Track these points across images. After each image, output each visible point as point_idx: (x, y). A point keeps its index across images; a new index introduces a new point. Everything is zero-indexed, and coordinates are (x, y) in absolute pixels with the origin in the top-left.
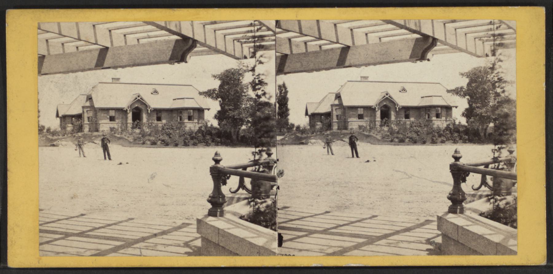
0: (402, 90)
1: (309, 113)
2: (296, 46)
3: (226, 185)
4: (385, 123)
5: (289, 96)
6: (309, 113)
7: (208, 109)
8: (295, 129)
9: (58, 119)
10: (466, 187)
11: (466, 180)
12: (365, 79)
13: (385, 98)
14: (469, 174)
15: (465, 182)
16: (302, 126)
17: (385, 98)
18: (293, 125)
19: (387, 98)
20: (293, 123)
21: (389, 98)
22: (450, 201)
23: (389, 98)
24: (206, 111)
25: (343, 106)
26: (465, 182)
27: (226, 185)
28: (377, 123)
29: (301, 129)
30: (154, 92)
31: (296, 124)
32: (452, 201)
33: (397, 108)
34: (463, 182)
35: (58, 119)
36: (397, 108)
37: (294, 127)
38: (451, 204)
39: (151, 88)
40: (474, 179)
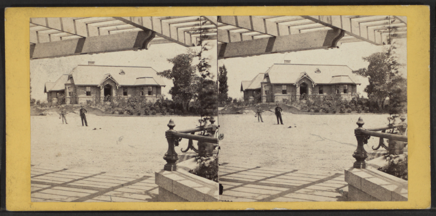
0: (317, 71)
1: (244, 89)
2: (233, 36)
3: (178, 146)
4: (108, 99)
5: (228, 75)
6: (244, 89)
7: (164, 86)
8: (232, 102)
9: (46, 94)
10: (367, 148)
11: (367, 142)
12: (287, 62)
13: (303, 77)
14: (370, 137)
15: (367, 144)
16: (238, 99)
17: (303, 77)
18: (231, 99)
19: (305, 77)
20: (231, 97)
21: (307, 77)
22: (355, 159)
23: (307, 77)
24: (162, 88)
25: (271, 83)
26: (367, 144)
27: (178, 146)
28: (297, 97)
29: (237, 101)
30: (121, 73)
31: (233, 98)
32: (357, 159)
33: (313, 85)
34: (365, 143)
35: (46, 94)
36: (313, 85)
37: (232, 100)
38: (355, 160)
39: (119, 70)
40: (373, 141)
